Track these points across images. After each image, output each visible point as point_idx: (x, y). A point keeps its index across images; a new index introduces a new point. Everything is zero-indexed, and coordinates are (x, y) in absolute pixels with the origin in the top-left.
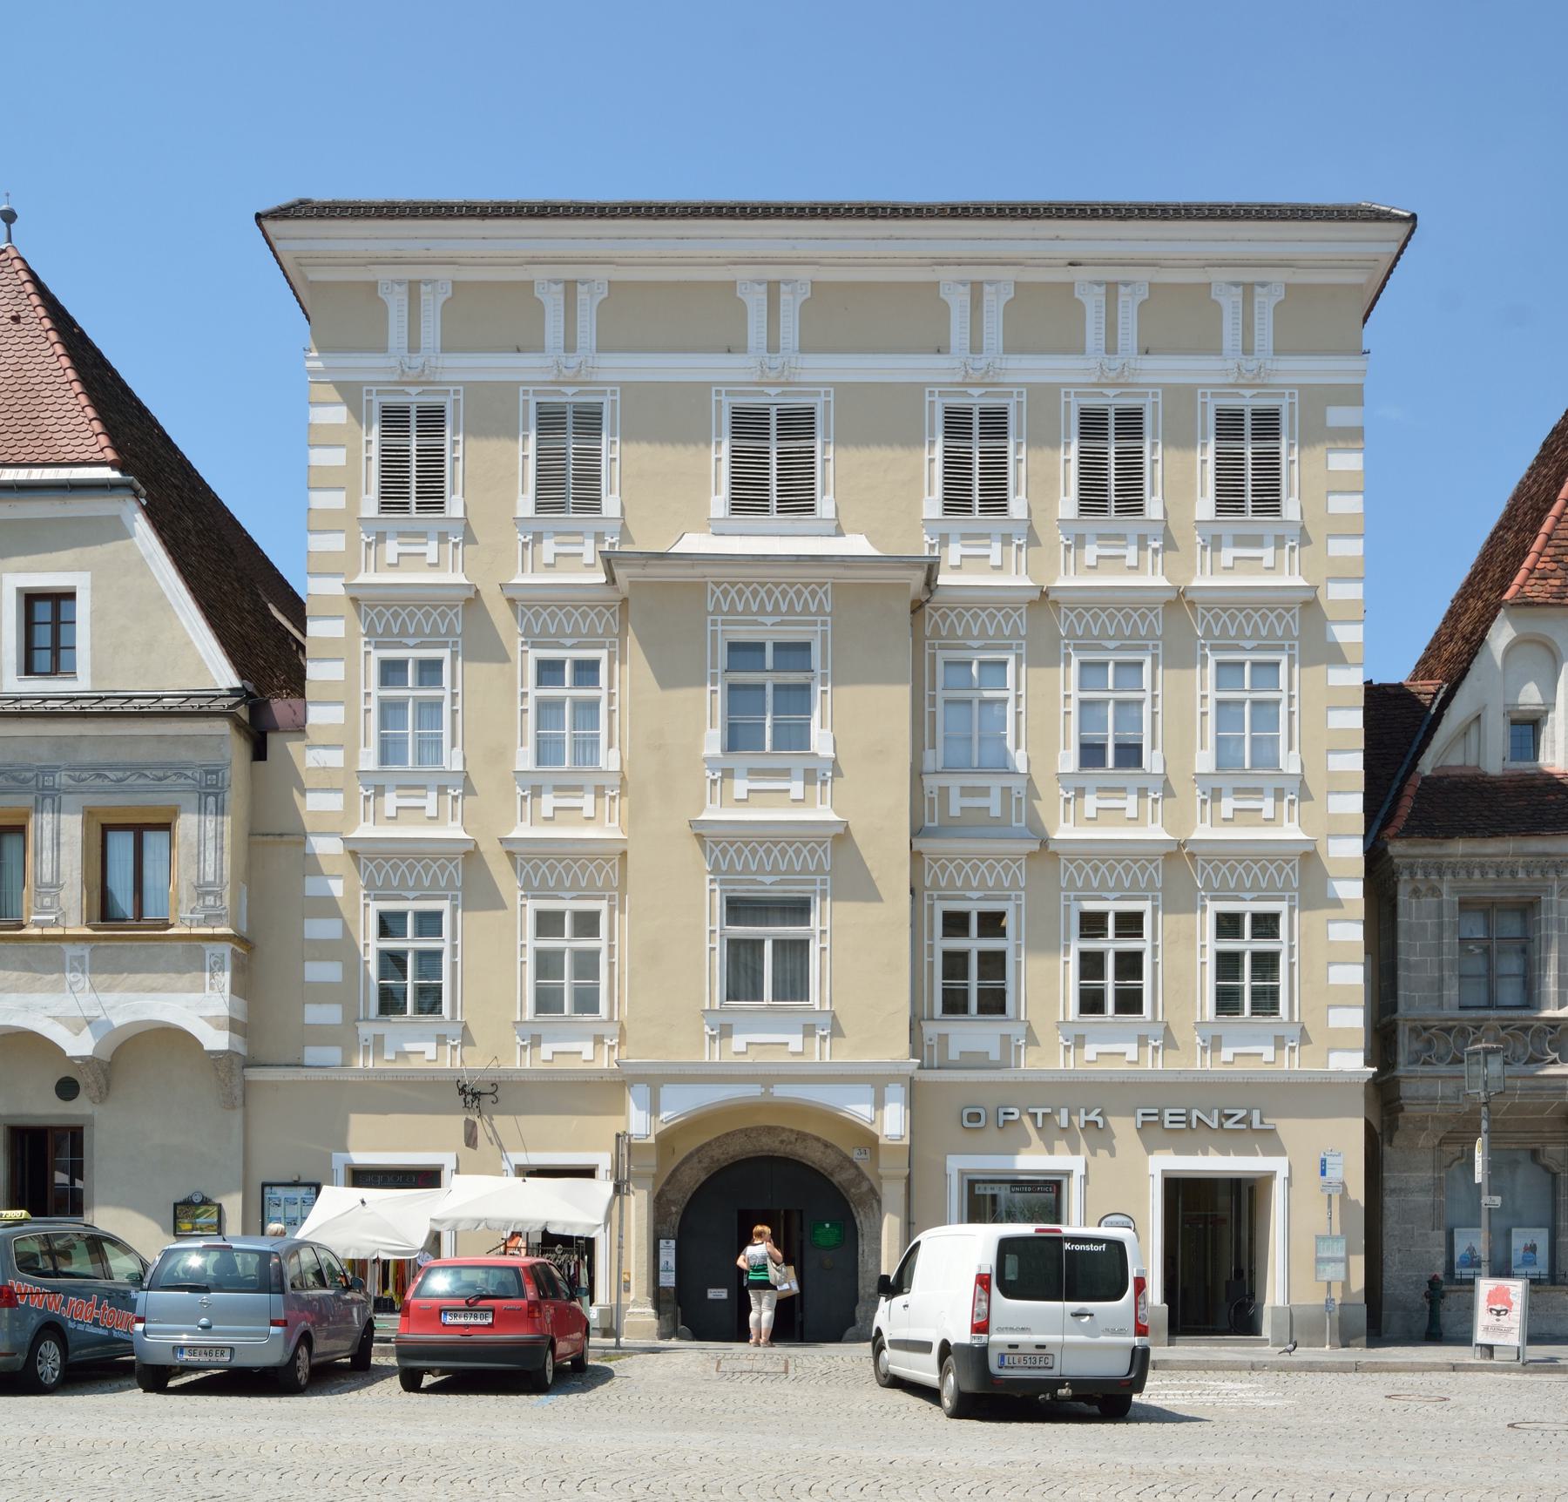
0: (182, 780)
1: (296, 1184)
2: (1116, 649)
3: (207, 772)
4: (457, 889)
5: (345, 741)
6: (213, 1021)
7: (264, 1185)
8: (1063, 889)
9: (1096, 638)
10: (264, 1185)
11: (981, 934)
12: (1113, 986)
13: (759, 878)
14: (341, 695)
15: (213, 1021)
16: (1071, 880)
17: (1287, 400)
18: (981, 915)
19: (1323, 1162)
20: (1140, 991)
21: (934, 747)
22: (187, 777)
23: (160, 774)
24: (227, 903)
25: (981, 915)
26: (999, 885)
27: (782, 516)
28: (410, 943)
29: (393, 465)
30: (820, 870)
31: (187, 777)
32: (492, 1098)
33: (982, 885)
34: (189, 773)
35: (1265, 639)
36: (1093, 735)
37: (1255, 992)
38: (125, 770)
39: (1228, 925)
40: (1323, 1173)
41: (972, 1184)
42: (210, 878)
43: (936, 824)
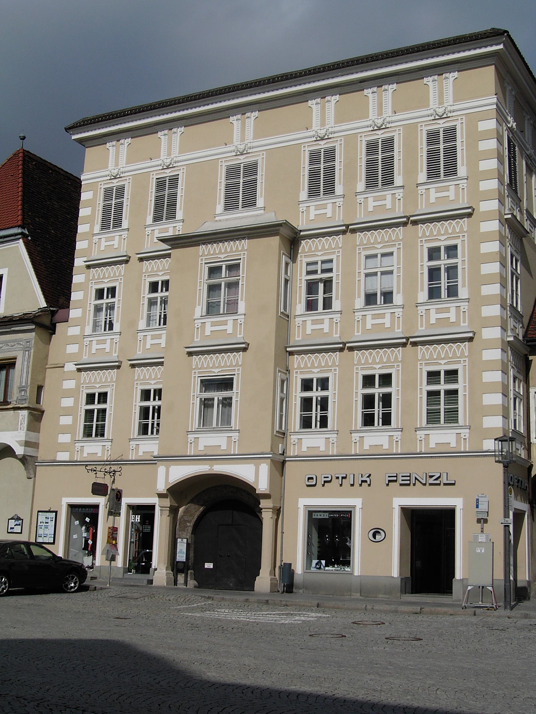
0: (19, 346)
1: (49, 511)
2: (381, 248)
3: (27, 342)
4: (466, 357)
5: (81, 322)
6: (19, 442)
7: (39, 512)
8: (355, 365)
9: (373, 244)
10: (39, 512)
11: (446, 382)
12: (376, 410)
13: (213, 370)
14: (82, 304)
15: (19, 442)
16: (359, 360)
17: (397, 132)
18: (380, 376)
19: (478, 500)
20: (312, 416)
21: (423, 291)
22: (21, 344)
23: (13, 344)
24: (28, 394)
25: (380, 376)
26: (327, 365)
27: (244, 209)
28: (377, 391)
29: (106, 210)
30: (237, 365)
31: (21, 344)
32: (119, 473)
33: (320, 366)
34: (21, 343)
35: (450, 234)
36: (313, 297)
37: (446, 411)
38: (2, 343)
39: (433, 376)
40: (477, 507)
41: (310, 513)
42: (24, 384)
43: (300, 339)
